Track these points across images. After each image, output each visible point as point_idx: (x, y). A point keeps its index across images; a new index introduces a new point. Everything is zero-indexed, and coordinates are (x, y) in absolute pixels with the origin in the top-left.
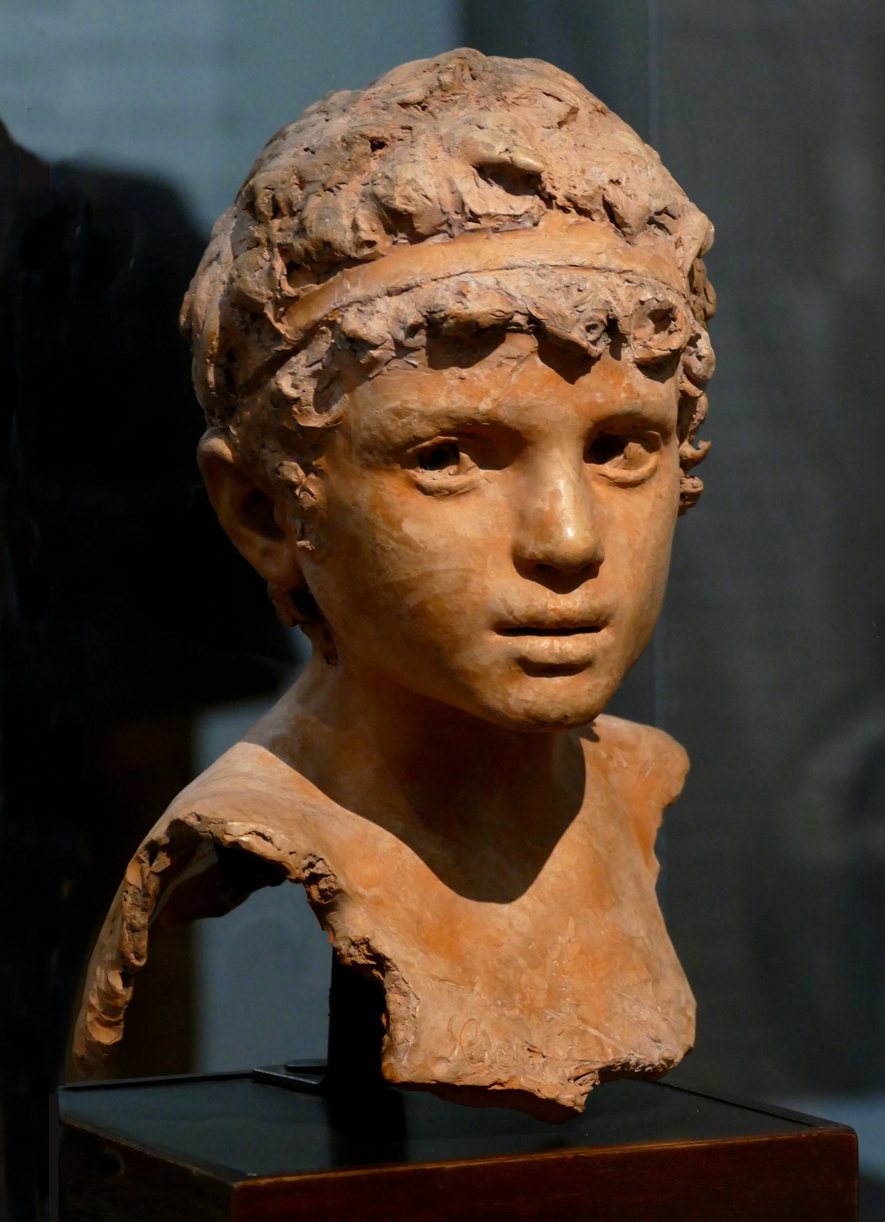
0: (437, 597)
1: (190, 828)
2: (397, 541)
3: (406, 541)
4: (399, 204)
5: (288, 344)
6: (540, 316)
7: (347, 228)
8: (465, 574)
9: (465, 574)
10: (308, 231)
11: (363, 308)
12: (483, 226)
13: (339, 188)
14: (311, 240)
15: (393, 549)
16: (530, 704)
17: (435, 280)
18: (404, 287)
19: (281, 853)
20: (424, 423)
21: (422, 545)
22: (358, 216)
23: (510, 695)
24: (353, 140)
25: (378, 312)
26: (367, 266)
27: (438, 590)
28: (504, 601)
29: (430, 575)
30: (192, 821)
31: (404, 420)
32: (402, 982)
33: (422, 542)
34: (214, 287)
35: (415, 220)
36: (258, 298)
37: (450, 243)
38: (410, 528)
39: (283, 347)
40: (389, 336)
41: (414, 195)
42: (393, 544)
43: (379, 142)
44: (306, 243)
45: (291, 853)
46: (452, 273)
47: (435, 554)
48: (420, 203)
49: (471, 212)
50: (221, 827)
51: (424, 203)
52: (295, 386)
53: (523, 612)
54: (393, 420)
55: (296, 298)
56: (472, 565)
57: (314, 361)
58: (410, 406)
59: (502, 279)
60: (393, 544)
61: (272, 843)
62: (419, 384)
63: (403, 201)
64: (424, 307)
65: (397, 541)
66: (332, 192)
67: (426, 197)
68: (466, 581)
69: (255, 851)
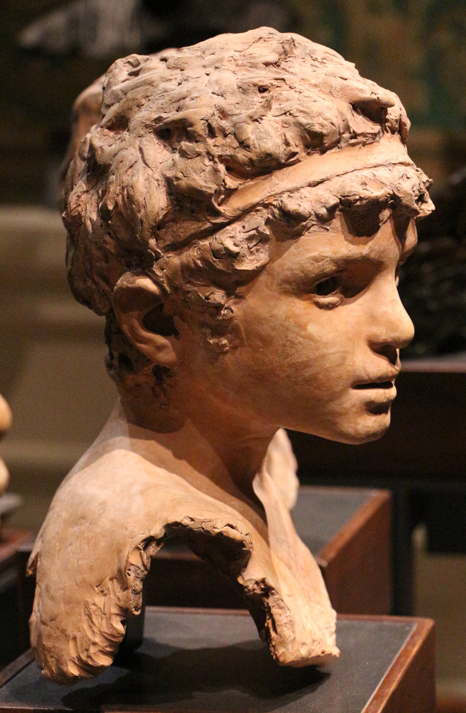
0: (327, 370)
1: (185, 526)
2: (303, 337)
3: (310, 338)
4: (317, 128)
5: (227, 218)
6: (400, 195)
7: (280, 144)
8: (344, 354)
9: (344, 354)
10: (252, 147)
11: (292, 195)
12: (359, 141)
13: (262, 119)
14: (256, 153)
15: (299, 342)
16: (370, 428)
17: (338, 176)
18: (320, 181)
19: (242, 535)
20: (332, 264)
21: (319, 339)
22: (288, 136)
23: (358, 424)
24: (249, 88)
25: (305, 197)
26: (290, 168)
27: (327, 365)
28: (364, 368)
29: (324, 356)
30: (186, 522)
31: (320, 264)
32: (280, 601)
33: (320, 337)
34: (149, 183)
35: (325, 138)
36: (208, 190)
37: (339, 151)
38: (312, 329)
39: (219, 220)
40: (313, 213)
41: (325, 122)
42: (300, 339)
43: (263, 89)
44: (250, 155)
45: (247, 535)
46: (348, 171)
47: (327, 343)
48: (329, 127)
49: (354, 131)
50: (210, 524)
51: (332, 128)
52: (235, 245)
53: (375, 374)
54: (312, 264)
55: (236, 190)
56: (348, 349)
57: (250, 229)
58: (324, 254)
59: (376, 173)
60: (300, 339)
61: (237, 530)
62: (330, 240)
63: (319, 126)
64: (338, 193)
65: (303, 337)
66: (258, 121)
67: (332, 123)
68: (344, 358)
69: (230, 536)
